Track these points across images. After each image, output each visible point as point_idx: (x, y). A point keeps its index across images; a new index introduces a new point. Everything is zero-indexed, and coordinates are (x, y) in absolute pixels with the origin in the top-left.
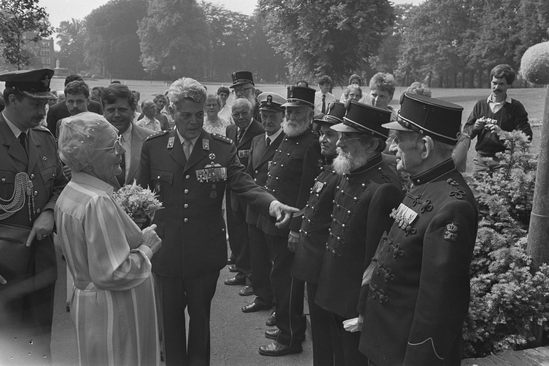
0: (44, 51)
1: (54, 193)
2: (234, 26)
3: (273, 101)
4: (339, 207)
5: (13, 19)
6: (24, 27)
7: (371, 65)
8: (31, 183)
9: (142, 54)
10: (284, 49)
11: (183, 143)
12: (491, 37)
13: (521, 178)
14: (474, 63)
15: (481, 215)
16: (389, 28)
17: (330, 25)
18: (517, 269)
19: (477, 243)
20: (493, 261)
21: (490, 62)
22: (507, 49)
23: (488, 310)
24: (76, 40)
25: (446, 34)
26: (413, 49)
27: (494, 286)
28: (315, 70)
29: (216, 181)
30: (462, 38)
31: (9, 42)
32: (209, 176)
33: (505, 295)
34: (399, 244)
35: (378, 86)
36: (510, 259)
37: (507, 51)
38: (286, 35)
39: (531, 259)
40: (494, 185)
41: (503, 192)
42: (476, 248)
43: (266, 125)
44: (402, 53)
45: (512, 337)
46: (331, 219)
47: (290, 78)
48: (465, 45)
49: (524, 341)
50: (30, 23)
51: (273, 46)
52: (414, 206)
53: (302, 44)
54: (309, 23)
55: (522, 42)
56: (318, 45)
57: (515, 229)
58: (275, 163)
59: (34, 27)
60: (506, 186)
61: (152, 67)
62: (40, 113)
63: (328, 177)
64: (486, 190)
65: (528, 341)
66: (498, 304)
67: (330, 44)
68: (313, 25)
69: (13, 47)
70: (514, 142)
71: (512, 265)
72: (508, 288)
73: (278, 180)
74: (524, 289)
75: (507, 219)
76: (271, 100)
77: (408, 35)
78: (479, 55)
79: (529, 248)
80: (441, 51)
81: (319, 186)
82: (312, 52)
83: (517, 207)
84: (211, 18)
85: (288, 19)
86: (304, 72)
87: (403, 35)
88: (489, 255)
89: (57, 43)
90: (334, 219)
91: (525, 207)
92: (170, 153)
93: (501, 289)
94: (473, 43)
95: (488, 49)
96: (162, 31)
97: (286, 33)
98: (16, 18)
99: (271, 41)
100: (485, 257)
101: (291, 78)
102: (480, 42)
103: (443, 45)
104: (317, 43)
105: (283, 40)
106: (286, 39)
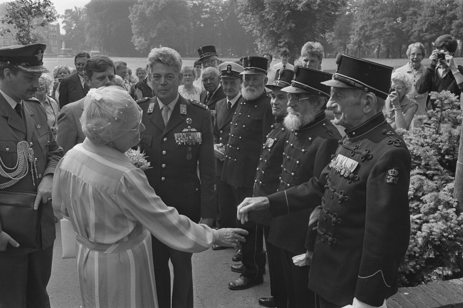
0: (52, 34)
1: (49, 158)
2: (210, 10)
3: (232, 70)
4: (289, 158)
5: (24, 8)
6: (33, 15)
7: (327, 40)
8: (31, 150)
9: (133, 35)
10: (253, 28)
11: (162, 109)
12: (431, 14)
13: (450, 133)
14: (417, 37)
15: (415, 164)
16: (343, 8)
17: (292, 6)
18: (445, 211)
19: (410, 188)
20: (424, 204)
21: (430, 36)
22: (445, 24)
23: (419, 246)
24: (78, 24)
25: (392, 12)
26: (364, 26)
27: (424, 225)
28: (279, 45)
29: (192, 144)
30: (406, 15)
31: (21, 27)
32: (186, 139)
33: (433, 233)
34: (343, 191)
35: (309, 52)
36: (438, 202)
37: (445, 26)
38: (254, 16)
39: (457, 202)
40: (426, 138)
41: (434, 144)
42: (410, 193)
43: (227, 90)
44: (354, 30)
45: (440, 269)
46: (282, 169)
47: (259, 53)
48: (409, 21)
49: (450, 273)
50: (38, 10)
51: (244, 26)
52: (353, 156)
53: (269, 24)
54: (273, 5)
55: (458, 18)
56: (281, 24)
57: (444, 176)
58: (236, 124)
59: (41, 14)
60: (437, 139)
61: (143, 46)
62: (34, 86)
63: (278, 134)
64: (419, 143)
65: (453, 272)
66: (428, 241)
67: (292, 22)
68: (277, 7)
69: (24, 32)
70: (444, 100)
71: (440, 207)
72: (437, 227)
73: (241, 139)
74: (450, 227)
75: (437, 168)
76: (231, 69)
77: (360, 14)
78: (420, 29)
79: (455, 192)
80: (387, 27)
81: (270, 142)
82: (277, 30)
83: (446, 157)
84: (191, 3)
85: (256, 3)
86: (270, 47)
87: (355, 14)
88: (421, 199)
89: (63, 28)
90: (285, 169)
91: (453, 157)
92: (149, 117)
93: (430, 228)
94: (416, 19)
95: (428, 25)
96: (150, 15)
97: (255, 15)
98: (26, 7)
99: (241, 21)
100: (418, 201)
101: (260, 53)
102: (421, 19)
103: (389, 22)
104: (281, 22)
105: (252, 21)
106: (255, 19)
